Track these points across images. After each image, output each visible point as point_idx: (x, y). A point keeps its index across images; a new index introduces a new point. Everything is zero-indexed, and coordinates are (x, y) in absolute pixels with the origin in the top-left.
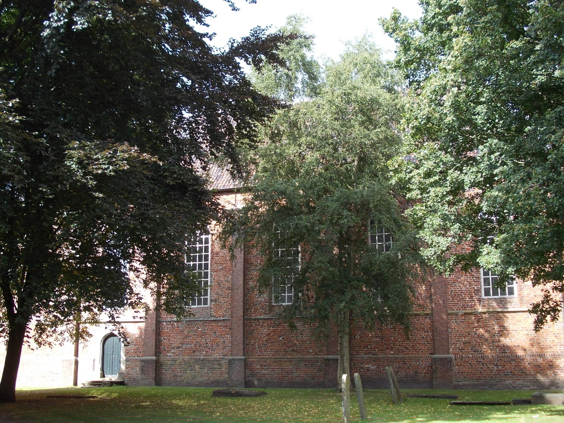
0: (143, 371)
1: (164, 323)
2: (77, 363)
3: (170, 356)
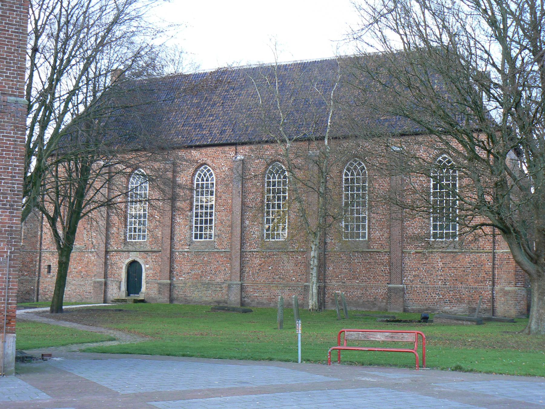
0: (160, 292)
1: (177, 253)
2: (106, 284)
3: (182, 280)
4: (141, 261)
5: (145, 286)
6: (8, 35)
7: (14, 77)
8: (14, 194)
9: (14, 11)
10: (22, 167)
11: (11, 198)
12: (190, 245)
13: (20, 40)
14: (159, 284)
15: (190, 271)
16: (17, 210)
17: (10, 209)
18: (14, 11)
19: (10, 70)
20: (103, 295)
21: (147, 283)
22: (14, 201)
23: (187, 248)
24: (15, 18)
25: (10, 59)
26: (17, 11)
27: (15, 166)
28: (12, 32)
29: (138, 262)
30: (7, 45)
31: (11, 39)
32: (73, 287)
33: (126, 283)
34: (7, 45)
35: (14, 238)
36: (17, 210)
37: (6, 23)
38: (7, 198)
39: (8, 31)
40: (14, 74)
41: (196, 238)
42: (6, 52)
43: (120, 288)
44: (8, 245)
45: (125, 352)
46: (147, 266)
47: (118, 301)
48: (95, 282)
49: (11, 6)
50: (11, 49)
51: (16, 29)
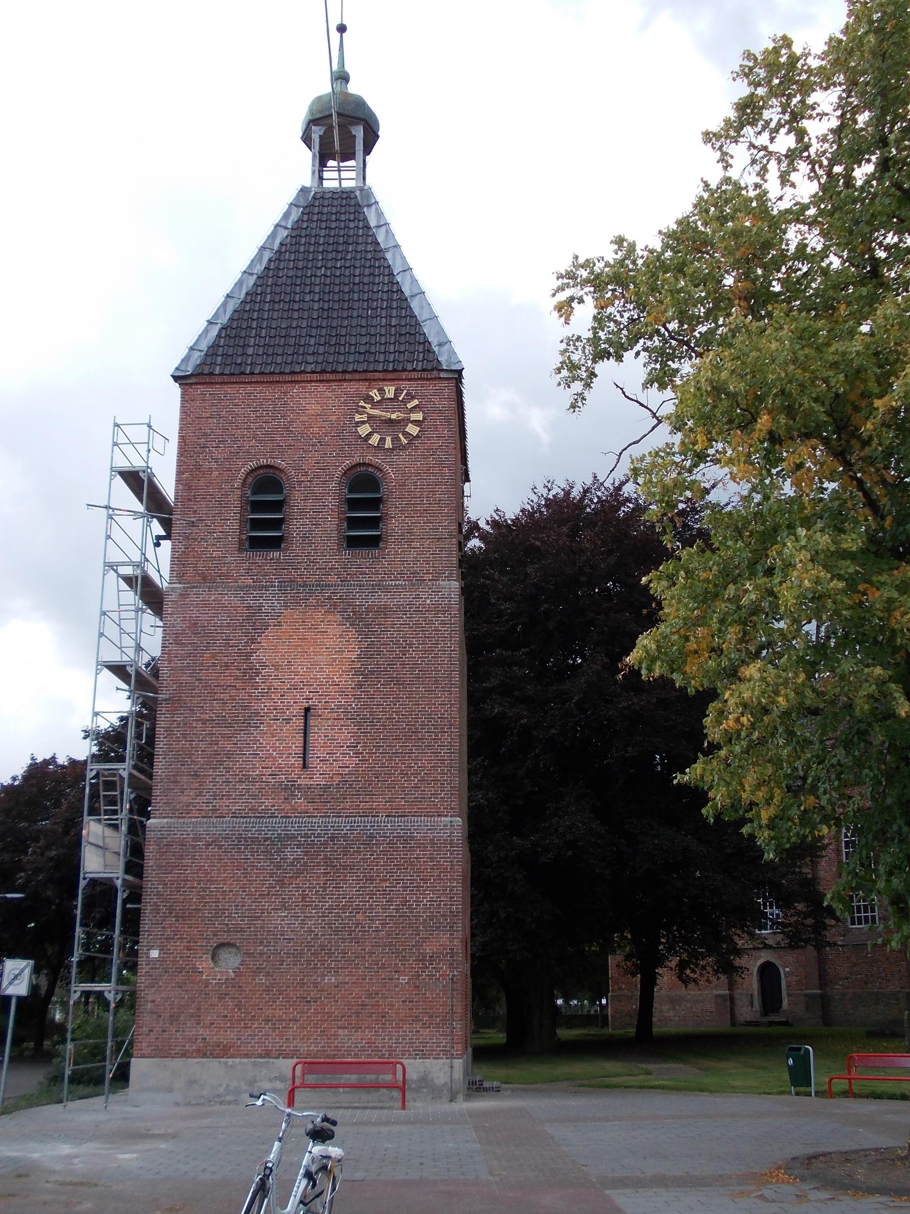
2: (732, 998)
4: (777, 963)
5: (787, 1000)
6: (441, 756)
7: (447, 798)
8: (453, 916)
9: (445, 732)
10: (460, 887)
11: (451, 919)
12: (844, 935)
13: (452, 760)
14: (806, 995)
15: (849, 976)
16: (457, 931)
17: (450, 931)
18: (445, 732)
19: (444, 791)
20: (729, 1016)
21: (789, 995)
22: (453, 923)
23: (841, 940)
24: (446, 739)
25: (444, 781)
26: (448, 732)
27: (453, 887)
28: (444, 753)
29: (773, 964)
30: (440, 767)
31: (444, 760)
32: (689, 1005)
33: (760, 997)
34: (440, 767)
35: (456, 960)
36: (457, 931)
37: (438, 746)
38: (447, 920)
39: (441, 753)
40: (448, 794)
41: (853, 923)
42: (439, 774)
43: (752, 1004)
44: (450, 968)
45: (662, 1087)
46: (787, 970)
47: (749, 1024)
48: (716, 996)
49: (442, 728)
50: (444, 770)
51: (448, 749)
